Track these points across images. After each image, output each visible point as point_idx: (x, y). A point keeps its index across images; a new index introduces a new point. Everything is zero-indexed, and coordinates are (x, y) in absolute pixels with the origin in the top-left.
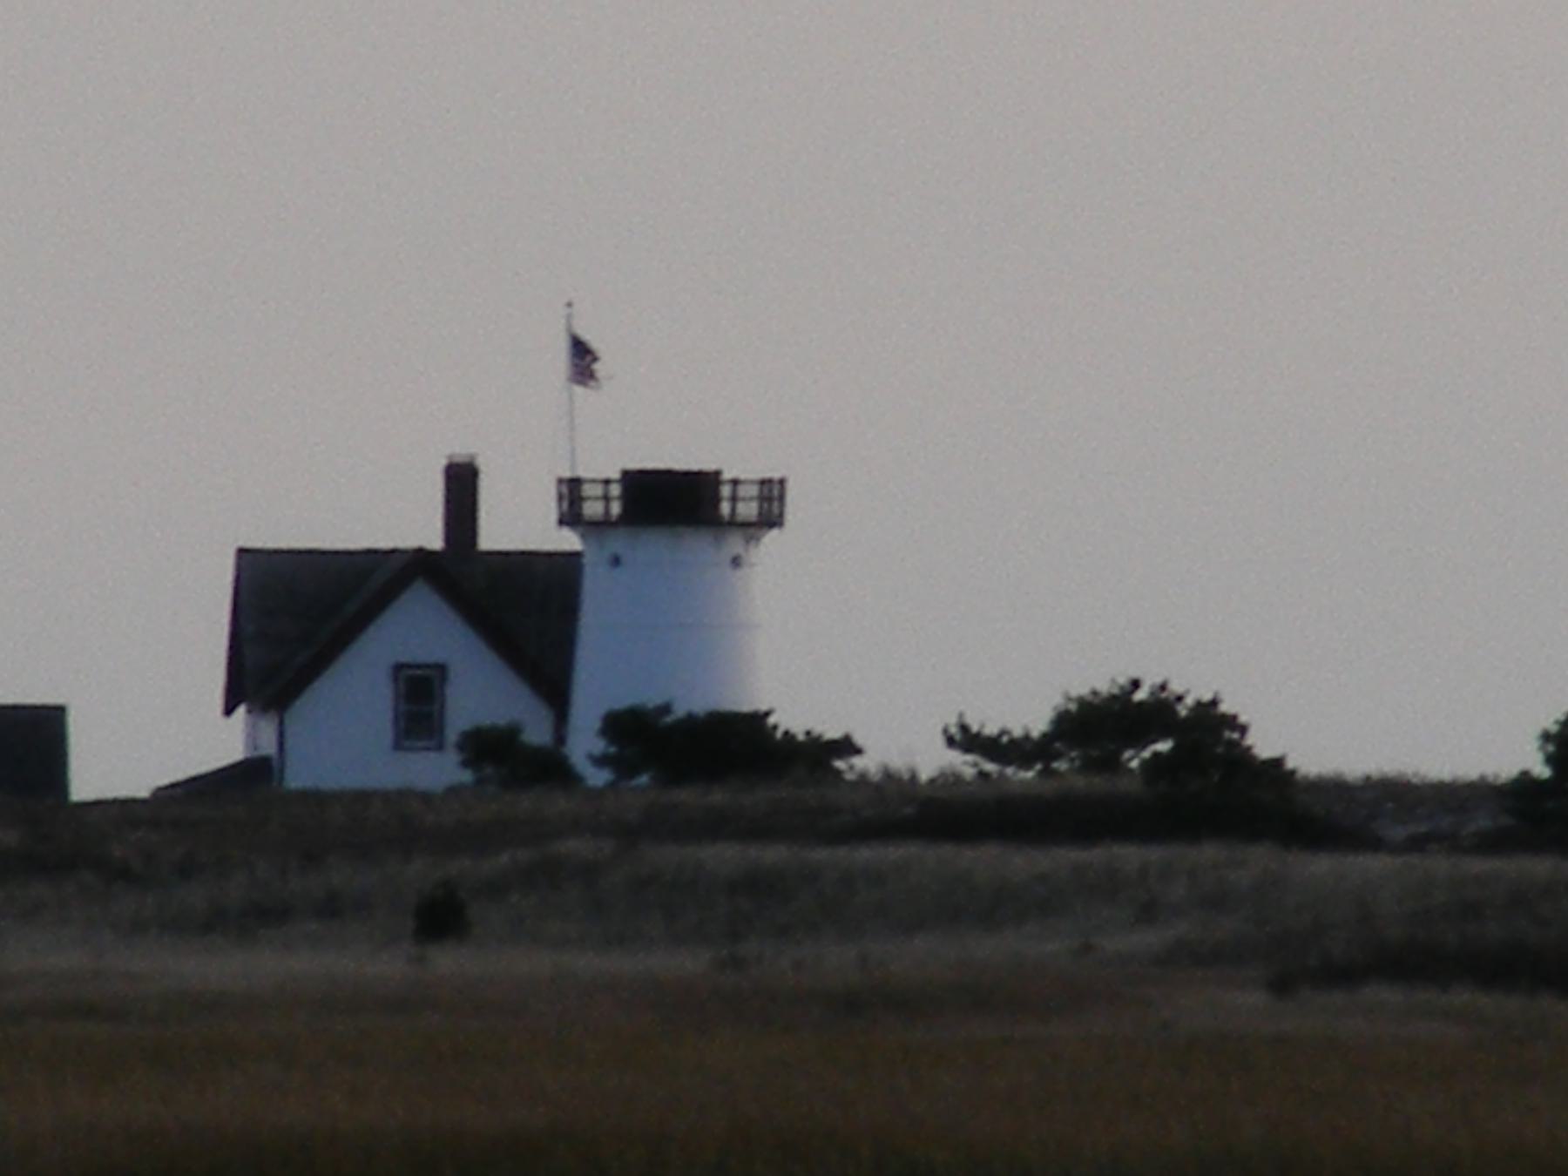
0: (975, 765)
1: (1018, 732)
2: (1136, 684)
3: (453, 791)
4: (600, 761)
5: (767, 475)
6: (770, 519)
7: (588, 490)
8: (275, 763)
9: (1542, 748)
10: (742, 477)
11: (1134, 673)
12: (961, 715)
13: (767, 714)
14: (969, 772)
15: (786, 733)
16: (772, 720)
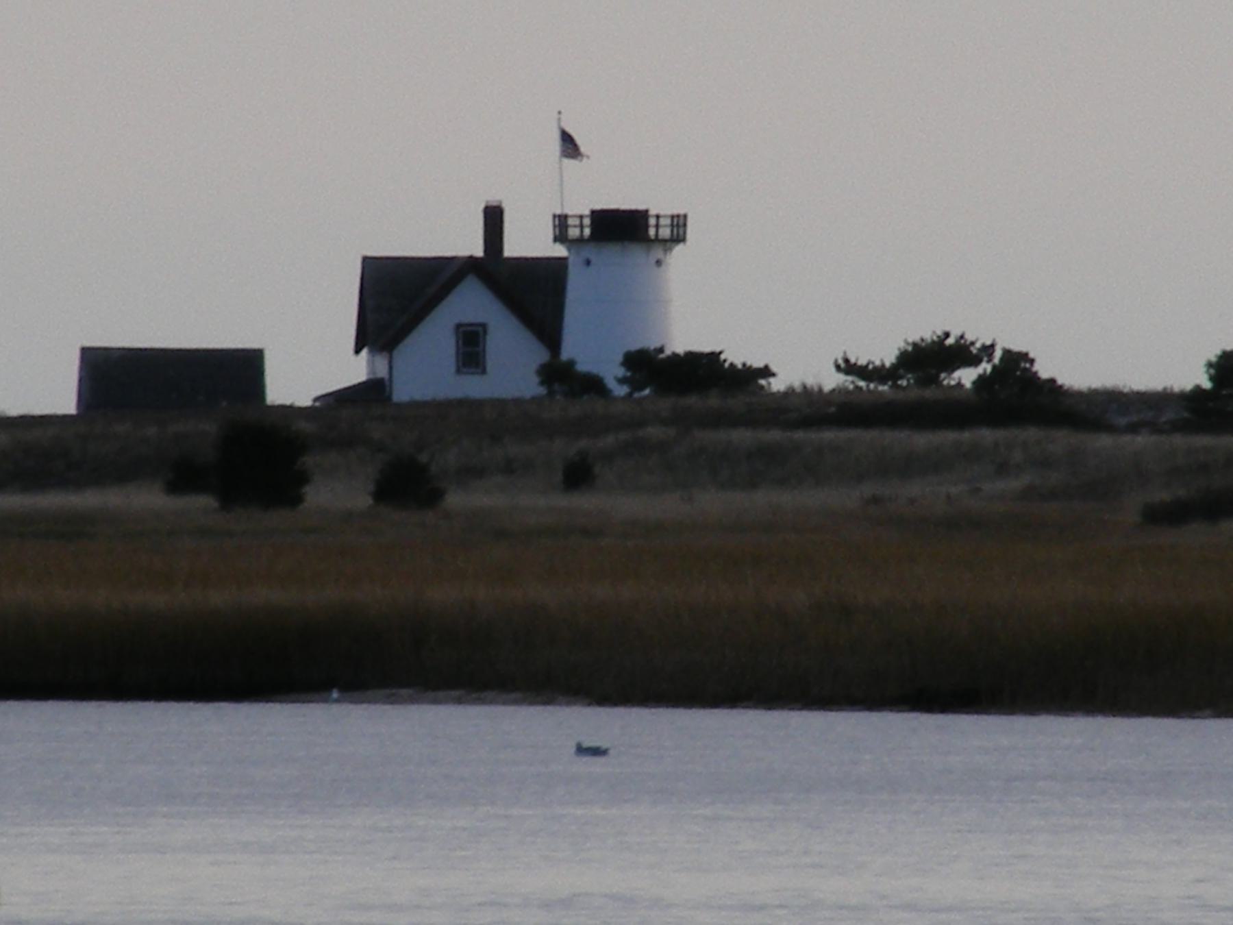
0: (853, 382)
1: (878, 363)
2: (947, 335)
4: (622, 381)
5: (675, 212)
6: (678, 238)
7: (571, 221)
8: (387, 383)
9: (1207, 372)
10: (662, 213)
12: (845, 353)
13: (720, 353)
15: (732, 365)
16: (723, 357)
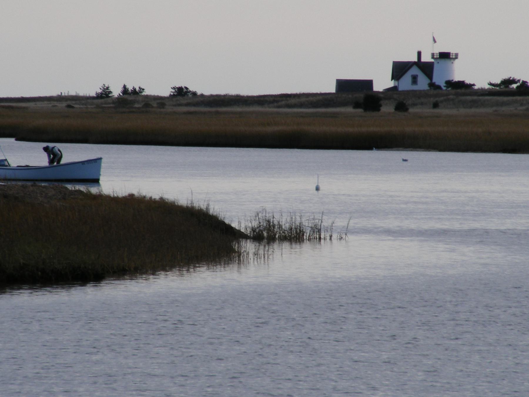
1: (497, 83)
2: (511, 77)
3: (428, 90)
4: (444, 86)
6: (456, 58)
7: (435, 54)
10: (453, 53)
11: (511, 76)
14: (491, 88)
